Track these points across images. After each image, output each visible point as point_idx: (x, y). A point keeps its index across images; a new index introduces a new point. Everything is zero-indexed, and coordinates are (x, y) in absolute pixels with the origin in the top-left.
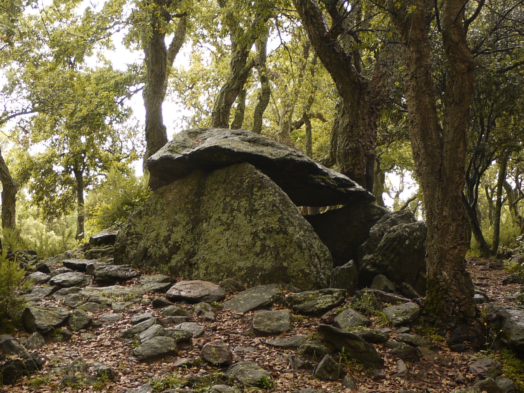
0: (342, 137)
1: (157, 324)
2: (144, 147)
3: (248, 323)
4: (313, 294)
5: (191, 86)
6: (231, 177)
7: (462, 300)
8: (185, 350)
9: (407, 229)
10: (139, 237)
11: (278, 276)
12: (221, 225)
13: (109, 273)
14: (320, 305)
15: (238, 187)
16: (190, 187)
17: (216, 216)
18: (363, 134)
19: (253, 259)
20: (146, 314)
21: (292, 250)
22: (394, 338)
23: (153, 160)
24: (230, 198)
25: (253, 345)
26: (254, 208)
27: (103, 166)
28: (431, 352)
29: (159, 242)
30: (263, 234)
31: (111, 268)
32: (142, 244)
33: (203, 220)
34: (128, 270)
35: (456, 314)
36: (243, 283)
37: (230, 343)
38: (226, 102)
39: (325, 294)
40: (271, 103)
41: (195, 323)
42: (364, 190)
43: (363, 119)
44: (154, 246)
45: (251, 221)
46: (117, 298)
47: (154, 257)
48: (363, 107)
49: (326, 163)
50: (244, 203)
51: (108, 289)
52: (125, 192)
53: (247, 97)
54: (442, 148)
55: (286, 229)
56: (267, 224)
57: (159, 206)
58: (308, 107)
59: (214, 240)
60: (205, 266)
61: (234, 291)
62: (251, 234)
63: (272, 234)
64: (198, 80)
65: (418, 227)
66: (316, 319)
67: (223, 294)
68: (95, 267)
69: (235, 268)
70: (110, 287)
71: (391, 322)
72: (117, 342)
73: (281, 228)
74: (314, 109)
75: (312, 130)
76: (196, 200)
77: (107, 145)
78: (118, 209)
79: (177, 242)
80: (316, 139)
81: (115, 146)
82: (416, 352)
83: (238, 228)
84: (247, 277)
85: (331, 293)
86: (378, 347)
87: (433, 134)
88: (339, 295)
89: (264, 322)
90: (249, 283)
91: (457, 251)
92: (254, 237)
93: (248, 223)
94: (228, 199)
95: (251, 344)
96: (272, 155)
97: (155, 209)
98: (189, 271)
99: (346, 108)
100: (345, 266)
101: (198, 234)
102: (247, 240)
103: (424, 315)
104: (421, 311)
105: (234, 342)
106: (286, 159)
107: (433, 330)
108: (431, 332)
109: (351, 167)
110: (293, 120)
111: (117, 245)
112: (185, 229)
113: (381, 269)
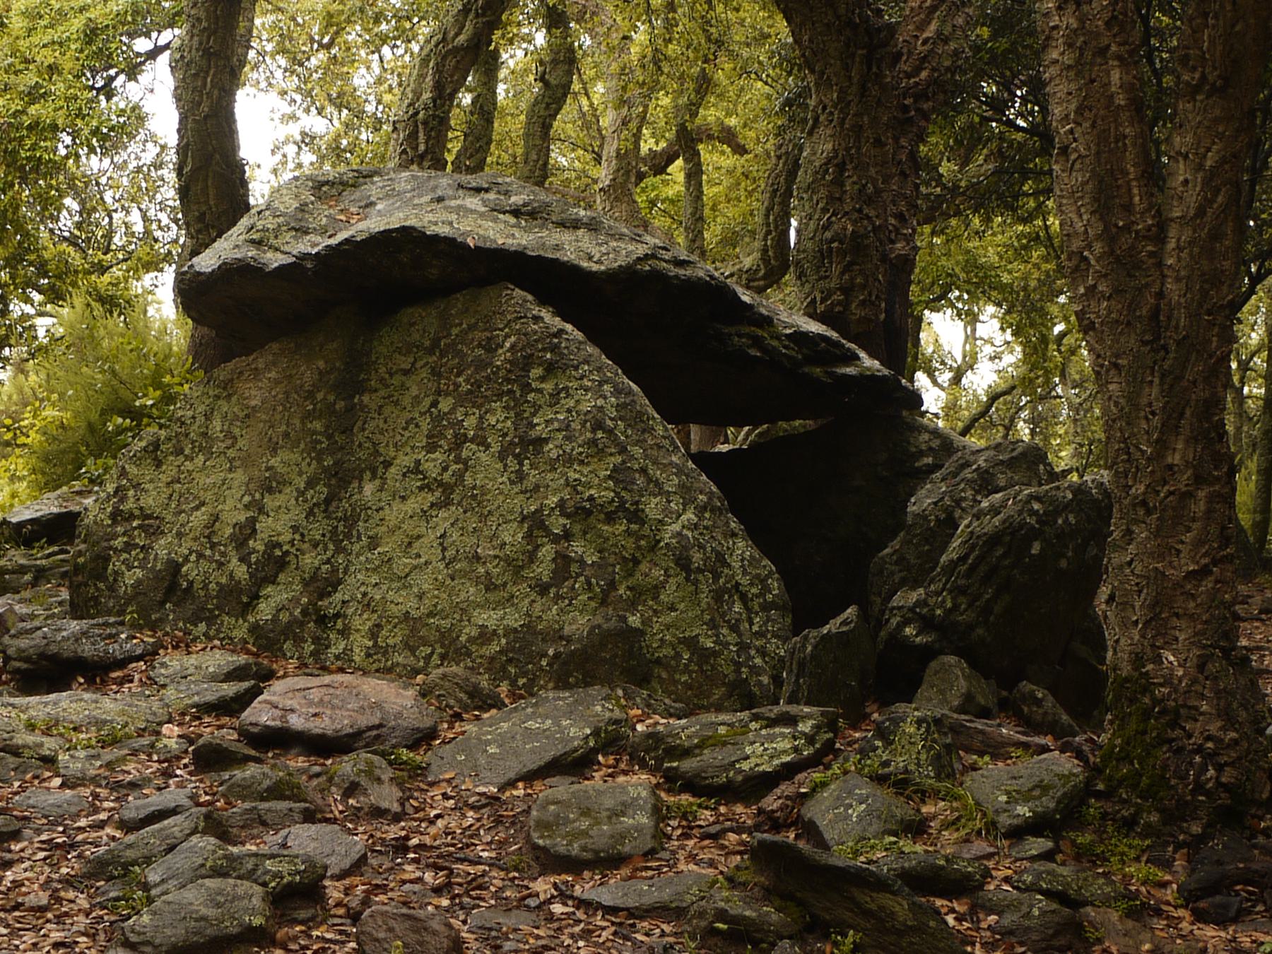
0: (811, 199)
1: (204, 833)
2: (180, 228)
3: (513, 823)
4: (731, 725)
5: (326, 40)
6: (455, 331)
7: (1228, 746)
8: (302, 923)
9: (1036, 506)
10: (152, 526)
11: (613, 660)
12: (421, 489)
13: (53, 649)
14: (753, 761)
15: (481, 365)
16: (321, 364)
17: (405, 461)
18: (878, 192)
19: (527, 601)
20: (173, 795)
21: (658, 573)
22: (1007, 880)
23: (199, 274)
24: (451, 400)
25: (532, 902)
26: (533, 434)
27: (52, 287)
28: (1130, 924)
29: (219, 544)
30: (563, 521)
31: (60, 630)
32: (162, 548)
33: (362, 471)
34: (117, 634)
35: (1208, 793)
36: (495, 681)
37: (453, 898)
38: (438, 87)
39: (772, 723)
40: (575, 94)
41: (337, 827)
42: (886, 372)
43: (878, 143)
44: (200, 556)
45: (520, 476)
46: (74, 737)
47: (202, 593)
48: (879, 102)
49: (749, 280)
50: (498, 417)
51: (46, 704)
52: (114, 373)
53: (503, 73)
54: (1161, 239)
55: (637, 503)
56: (574, 488)
57: (217, 424)
58: (693, 108)
59: (399, 537)
60: (369, 624)
61: (466, 708)
62: (522, 522)
63: (592, 520)
64: (348, 21)
65: (1070, 496)
66: (739, 809)
67: (428, 723)
68: (10, 624)
69: (469, 631)
70: (53, 696)
71: (994, 823)
72: (71, 894)
73: (623, 502)
74: (710, 114)
75: (704, 177)
76: (340, 405)
77: (66, 223)
78: (91, 427)
79: (279, 545)
80: (714, 209)
81: (90, 224)
82: (1080, 926)
83: (477, 499)
84: (510, 661)
85: (791, 720)
86: (952, 911)
87: (1136, 191)
88: (817, 727)
89: (567, 821)
90: (513, 683)
91: (1208, 583)
92: (530, 530)
93: (512, 482)
94: (445, 405)
95: (524, 898)
96: (590, 258)
97: (205, 434)
98: (316, 640)
99: (824, 108)
100: (832, 626)
101: (345, 519)
102: (508, 539)
103: (1098, 795)
104: (1089, 783)
105: (467, 893)
106: (636, 272)
107: (1130, 847)
108: (1123, 854)
109: (838, 297)
110: (644, 148)
111: (80, 553)
112: (306, 501)
113: (949, 635)
